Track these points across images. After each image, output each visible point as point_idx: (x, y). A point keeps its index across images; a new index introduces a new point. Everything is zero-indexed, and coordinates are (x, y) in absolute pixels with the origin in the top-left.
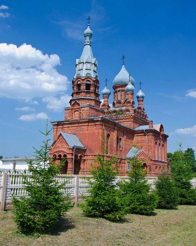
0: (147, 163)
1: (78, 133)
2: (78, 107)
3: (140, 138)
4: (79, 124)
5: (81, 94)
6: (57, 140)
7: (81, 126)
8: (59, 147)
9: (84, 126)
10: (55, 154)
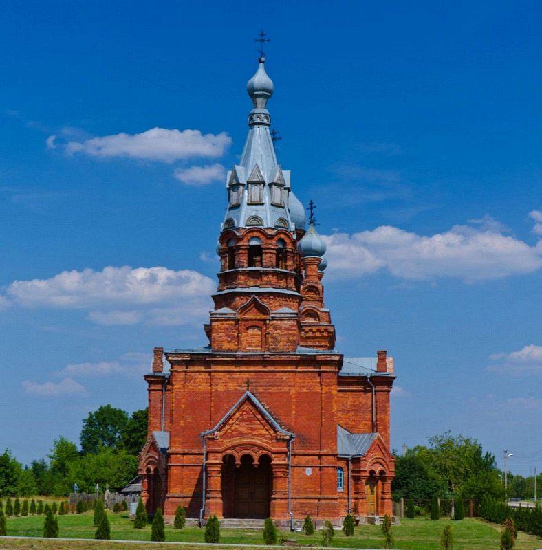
0: (387, 471)
1: (261, 390)
2: (258, 317)
3: (352, 399)
4: (265, 367)
5: (265, 279)
6: (234, 414)
7: (272, 372)
8: (241, 434)
9: (283, 372)
10: (229, 452)
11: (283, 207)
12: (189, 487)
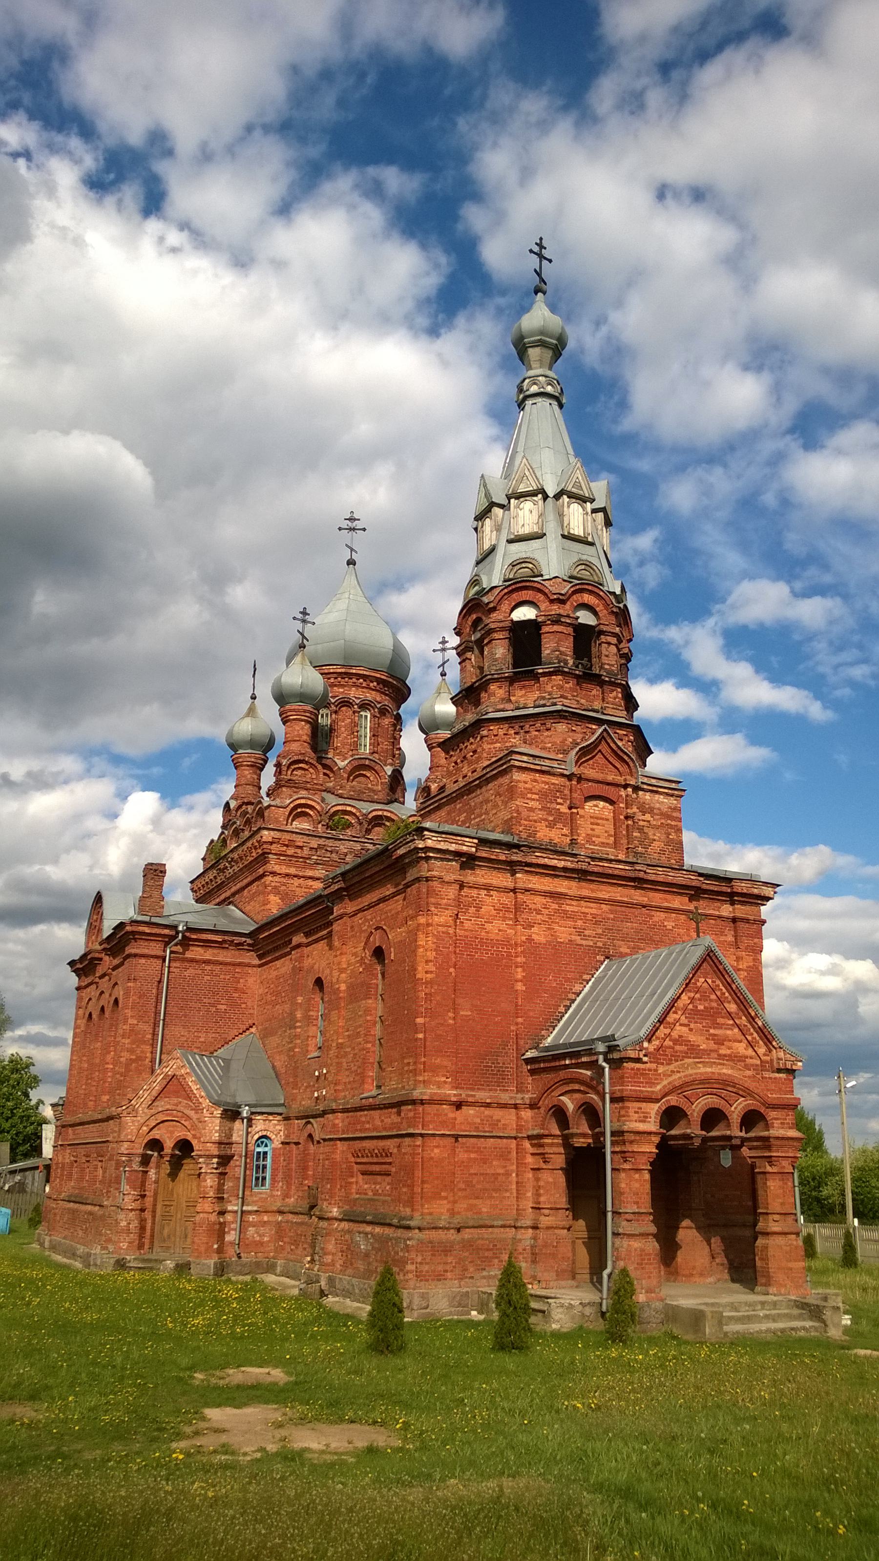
8: (693, 1051)
11: (592, 544)
12: (466, 1197)
